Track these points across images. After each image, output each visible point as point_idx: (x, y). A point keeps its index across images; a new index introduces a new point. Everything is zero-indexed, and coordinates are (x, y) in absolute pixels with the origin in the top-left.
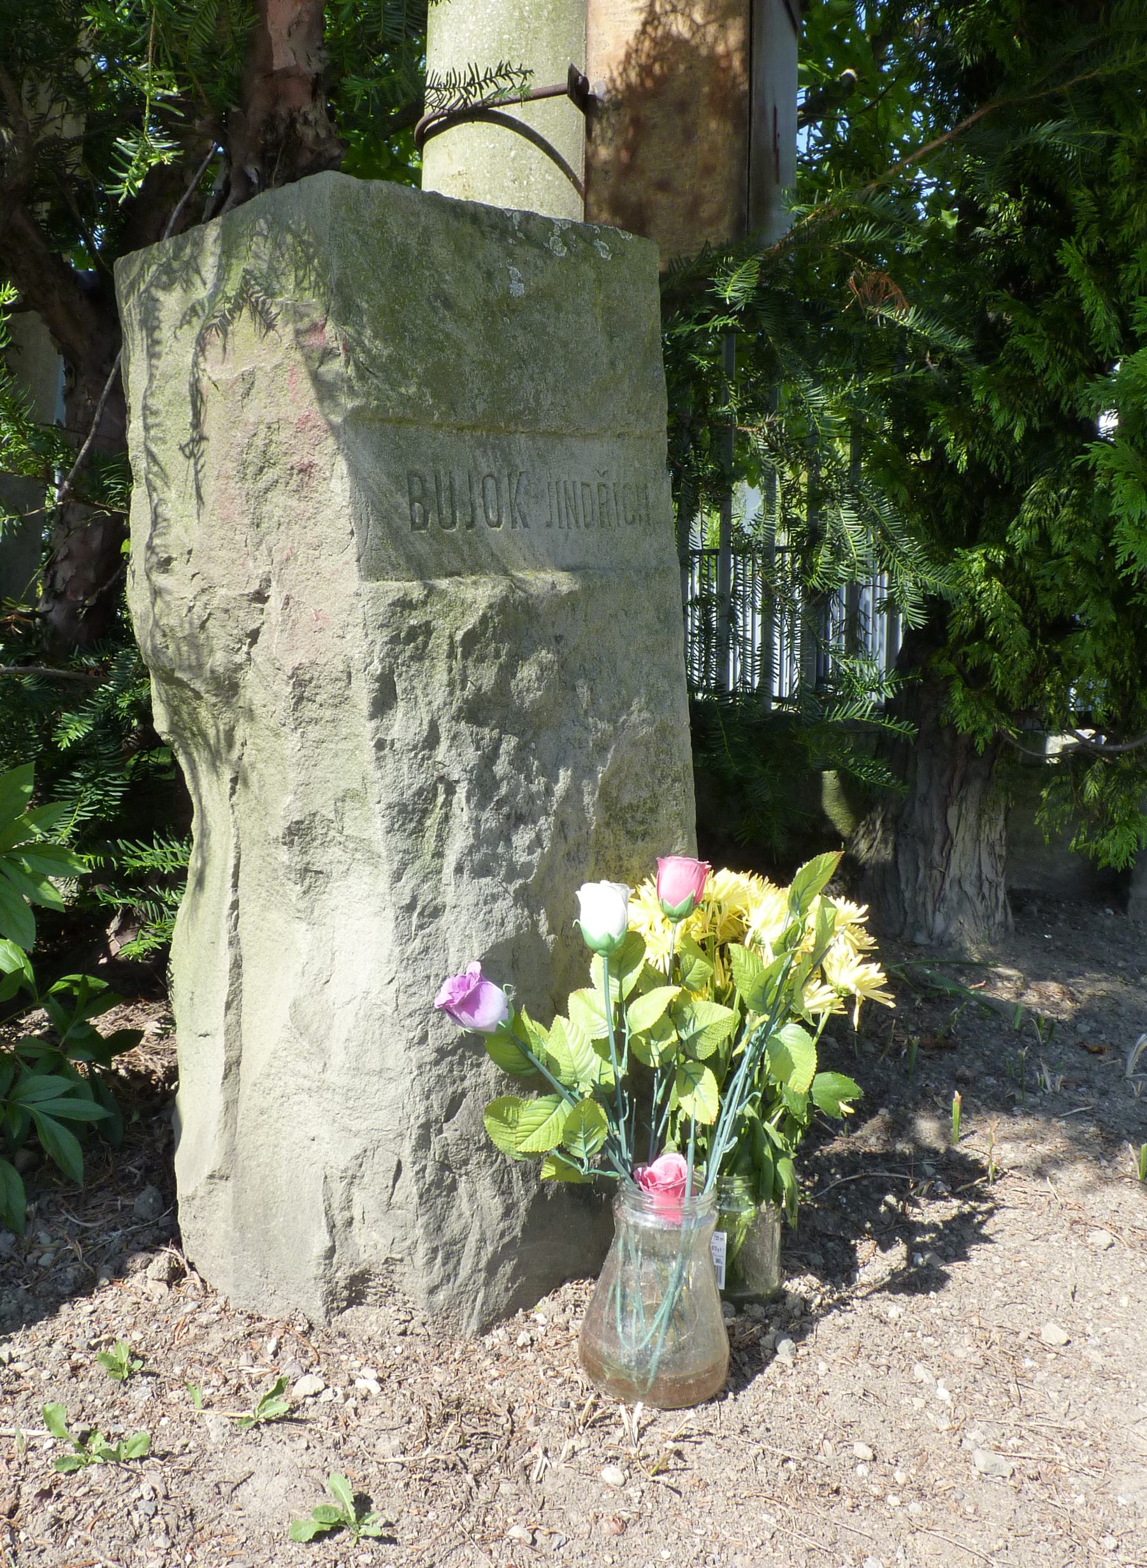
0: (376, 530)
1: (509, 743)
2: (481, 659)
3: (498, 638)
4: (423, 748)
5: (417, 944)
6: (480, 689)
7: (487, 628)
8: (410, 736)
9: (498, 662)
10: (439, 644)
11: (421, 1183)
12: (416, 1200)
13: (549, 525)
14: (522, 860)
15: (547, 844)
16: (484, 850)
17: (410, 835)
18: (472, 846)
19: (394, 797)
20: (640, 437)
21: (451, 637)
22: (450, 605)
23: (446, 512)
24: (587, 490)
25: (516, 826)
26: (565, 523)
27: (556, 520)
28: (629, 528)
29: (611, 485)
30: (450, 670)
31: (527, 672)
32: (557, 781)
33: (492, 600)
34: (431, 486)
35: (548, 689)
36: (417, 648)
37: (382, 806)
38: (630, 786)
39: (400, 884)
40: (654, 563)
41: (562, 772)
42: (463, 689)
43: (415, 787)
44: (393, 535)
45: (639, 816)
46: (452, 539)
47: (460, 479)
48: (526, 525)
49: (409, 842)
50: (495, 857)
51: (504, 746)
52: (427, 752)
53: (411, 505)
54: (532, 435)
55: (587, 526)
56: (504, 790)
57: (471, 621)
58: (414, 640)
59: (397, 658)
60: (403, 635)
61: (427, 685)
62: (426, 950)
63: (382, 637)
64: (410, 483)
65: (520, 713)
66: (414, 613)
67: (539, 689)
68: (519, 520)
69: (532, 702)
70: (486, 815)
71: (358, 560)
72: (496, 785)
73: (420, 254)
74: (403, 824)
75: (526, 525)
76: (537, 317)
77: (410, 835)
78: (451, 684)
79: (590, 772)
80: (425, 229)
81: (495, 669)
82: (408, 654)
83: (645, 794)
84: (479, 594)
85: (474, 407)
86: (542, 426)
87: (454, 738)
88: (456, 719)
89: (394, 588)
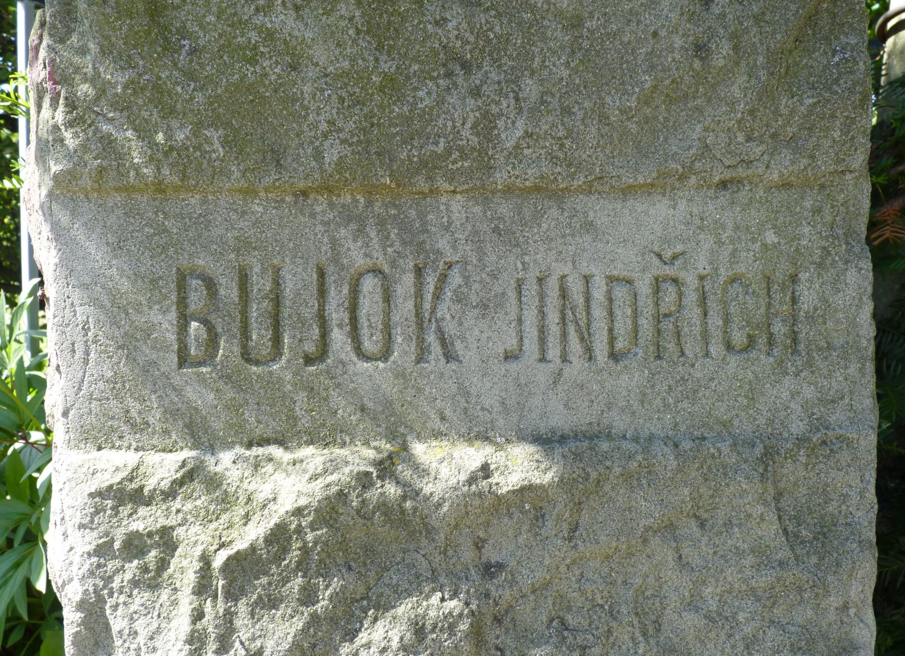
2: (271, 602)
3: (313, 566)
7: (285, 550)
9: (307, 611)
10: (184, 569)
13: (509, 356)
20: (786, 185)
21: (206, 560)
22: (226, 501)
23: (259, 336)
24: (620, 293)
26: (554, 353)
27: (531, 346)
28: (733, 361)
29: (690, 280)
30: (198, 615)
33: (303, 502)
34: (229, 291)
36: (145, 569)
40: (798, 427)
47: (296, 280)
48: (449, 356)
53: (183, 328)
54: (483, 194)
55: (614, 356)
57: (253, 533)
58: (141, 553)
59: (109, 580)
60: (117, 545)
61: (158, 630)
66: (142, 511)
68: (436, 349)
75: (449, 356)
81: (298, 623)
82: (128, 576)
84: (288, 483)
85: (318, 155)
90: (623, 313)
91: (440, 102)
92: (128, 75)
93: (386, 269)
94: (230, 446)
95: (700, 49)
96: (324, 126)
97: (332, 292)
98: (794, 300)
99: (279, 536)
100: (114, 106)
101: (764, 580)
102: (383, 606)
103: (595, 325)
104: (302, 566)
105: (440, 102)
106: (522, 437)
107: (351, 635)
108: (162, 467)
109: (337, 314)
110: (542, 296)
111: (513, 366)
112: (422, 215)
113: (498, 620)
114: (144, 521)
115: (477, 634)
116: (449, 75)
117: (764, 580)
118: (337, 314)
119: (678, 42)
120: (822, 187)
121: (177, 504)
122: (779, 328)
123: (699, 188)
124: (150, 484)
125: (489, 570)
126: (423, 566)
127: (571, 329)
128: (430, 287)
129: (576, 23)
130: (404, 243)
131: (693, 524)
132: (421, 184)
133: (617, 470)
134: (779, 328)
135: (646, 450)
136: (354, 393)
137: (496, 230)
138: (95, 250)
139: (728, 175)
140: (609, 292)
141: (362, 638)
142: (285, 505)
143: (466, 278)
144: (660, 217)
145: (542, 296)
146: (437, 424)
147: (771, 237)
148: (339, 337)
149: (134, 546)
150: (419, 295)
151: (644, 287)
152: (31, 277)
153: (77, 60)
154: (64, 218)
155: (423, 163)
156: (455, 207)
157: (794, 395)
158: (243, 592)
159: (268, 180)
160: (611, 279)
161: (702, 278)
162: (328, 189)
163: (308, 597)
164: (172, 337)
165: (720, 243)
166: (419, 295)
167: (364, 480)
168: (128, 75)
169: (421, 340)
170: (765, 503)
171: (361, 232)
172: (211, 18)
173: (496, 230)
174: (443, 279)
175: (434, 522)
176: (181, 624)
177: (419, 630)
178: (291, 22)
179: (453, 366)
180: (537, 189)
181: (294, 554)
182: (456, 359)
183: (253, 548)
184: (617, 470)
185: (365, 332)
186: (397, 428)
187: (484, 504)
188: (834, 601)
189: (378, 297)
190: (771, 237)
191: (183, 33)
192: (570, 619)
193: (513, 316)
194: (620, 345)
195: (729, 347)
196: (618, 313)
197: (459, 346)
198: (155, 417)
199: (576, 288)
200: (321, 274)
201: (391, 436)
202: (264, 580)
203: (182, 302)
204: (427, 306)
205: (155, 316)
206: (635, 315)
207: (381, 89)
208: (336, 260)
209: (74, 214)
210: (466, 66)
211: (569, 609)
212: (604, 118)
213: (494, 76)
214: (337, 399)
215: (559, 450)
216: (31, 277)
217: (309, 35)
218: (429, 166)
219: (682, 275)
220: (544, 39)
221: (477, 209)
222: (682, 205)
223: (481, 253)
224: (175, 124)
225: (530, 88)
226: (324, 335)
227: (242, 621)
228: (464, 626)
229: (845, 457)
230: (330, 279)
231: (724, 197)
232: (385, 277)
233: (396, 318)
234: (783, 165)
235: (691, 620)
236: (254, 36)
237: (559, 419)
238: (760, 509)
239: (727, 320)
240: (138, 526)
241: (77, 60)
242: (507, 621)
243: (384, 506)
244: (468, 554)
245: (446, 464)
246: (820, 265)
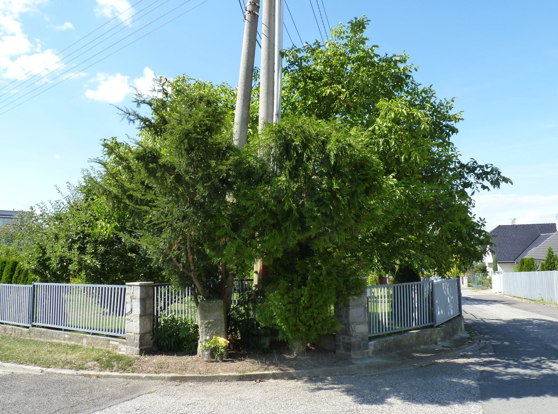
84: (207, 321)
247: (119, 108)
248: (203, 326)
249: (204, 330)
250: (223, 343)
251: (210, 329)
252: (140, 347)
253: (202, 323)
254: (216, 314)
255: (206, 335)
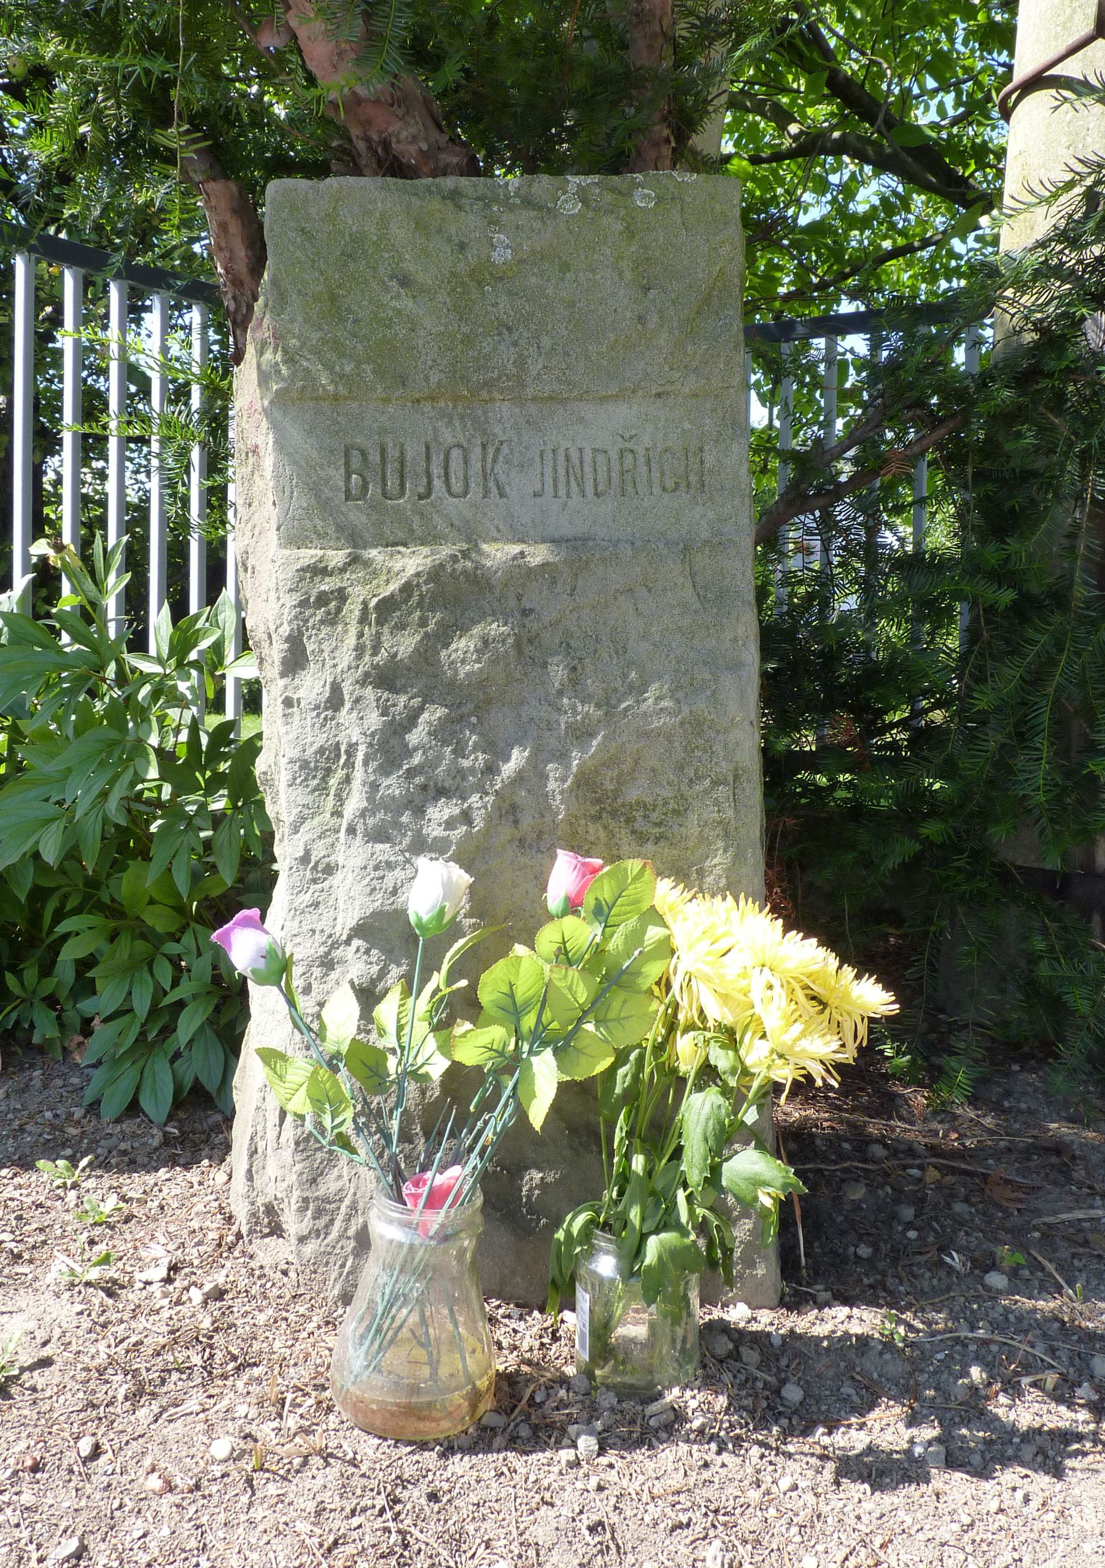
0: (301, 500)
1: (434, 714)
2: (402, 626)
3: (428, 604)
4: (326, 709)
5: (307, 898)
6: (396, 655)
7: (410, 596)
8: (313, 696)
10: (352, 609)
11: (299, 1130)
12: (293, 1146)
14: (435, 833)
15: (479, 823)
16: (380, 815)
17: (314, 790)
18: (365, 809)
19: (295, 753)
21: (365, 603)
22: (375, 574)
23: (392, 483)
24: (600, 458)
25: (436, 799)
26: (562, 492)
27: (549, 489)
28: (666, 496)
29: (641, 451)
30: (361, 635)
31: (463, 645)
32: (507, 759)
33: (420, 569)
34: (375, 457)
35: (494, 662)
36: (329, 613)
37: (286, 760)
38: (643, 781)
39: (297, 836)
40: (705, 535)
41: (515, 752)
42: (375, 653)
43: (316, 746)
44: (324, 506)
45: (655, 816)
46: (398, 510)
47: (414, 451)
49: (310, 798)
50: (397, 825)
51: (425, 716)
52: (329, 713)
55: (597, 495)
56: (417, 759)
57: (394, 587)
58: (326, 604)
59: (307, 621)
61: (336, 648)
62: (316, 905)
63: (291, 600)
64: (347, 455)
65: (452, 683)
66: (327, 579)
67: (478, 661)
68: (494, 491)
69: (468, 674)
70: (391, 780)
71: (278, 529)
72: (409, 753)
73: (380, 239)
74: (306, 780)
76: (533, 280)
77: (314, 790)
78: (359, 649)
79: (563, 757)
80: (382, 215)
82: (318, 618)
83: (666, 793)
84: (411, 562)
85: (427, 379)
86: (530, 392)
87: (357, 701)
88: (363, 682)
89: (309, 555)
90: (602, 470)
91: (495, 349)
92: (319, 335)
93: (465, 445)
94: (376, 546)
95: (641, 319)
96: (430, 363)
97: (434, 458)
98: (702, 462)
99: (407, 588)
100: (310, 351)
101: (686, 621)
102: (465, 630)
103: (586, 476)
104: (420, 604)
105: (495, 349)
106: (544, 541)
107: (447, 646)
108: (337, 557)
109: (436, 470)
110: (555, 460)
111: (538, 500)
112: (485, 413)
113: (530, 641)
114: (327, 585)
115: (518, 646)
116: (500, 334)
117: (686, 621)
118: (436, 470)
119: (628, 315)
120: (716, 396)
121: (348, 575)
122: (693, 478)
123: (644, 397)
124: (331, 565)
125: (525, 613)
126: (487, 608)
127: (572, 478)
128: (491, 451)
129: (571, 305)
130: (475, 429)
131: (645, 590)
132: (484, 394)
133: (598, 556)
134: (693, 478)
135: (615, 546)
136: (447, 516)
137: (528, 422)
138: (296, 435)
139: (660, 390)
140: (594, 457)
141: (453, 646)
142: (411, 571)
143: (511, 450)
144: (622, 413)
145: (555, 460)
146: (495, 534)
147: (687, 425)
148: (438, 483)
149: (323, 599)
150: (484, 460)
151: (614, 455)
152: (24, 574)
153: (289, 326)
154: (278, 415)
155: (486, 383)
156: (504, 409)
157: (703, 516)
158: (386, 621)
159: (398, 393)
160: (595, 450)
161: (647, 449)
162: (432, 398)
163: (423, 622)
164: (341, 484)
165: (657, 429)
166: (484, 460)
167: (454, 558)
168: (319, 335)
169: (485, 487)
170: (685, 577)
171: (450, 422)
172: (365, 303)
173: (528, 422)
174: (498, 450)
175: (493, 582)
176: (351, 641)
177: (486, 642)
178: (410, 304)
179: (505, 500)
180: (551, 398)
181: (415, 599)
182: (506, 496)
183: (392, 595)
184: (598, 556)
185: (453, 480)
186: (472, 538)
187: (521, 574)
188: (728, 635)
189: (461, 461)
190: (687, 425)
191: (349, 311)
192: (572, 643)
193: (539, 471)
194: (600, 488)
195: (664, 489)
196: (599, 470)
197: (507, 488)
198: (331, 530)
199: (574, 455)
200: (428, 448)
201: (469, 540)
202: (398, 613)
203: (347, 464)
204: (489, 466)
205: (331, 472)
206: (609, 470)
207: (462, 342)
208: (436, 439)
209: (285, 413)
210: (509, 329)
211: (572, 637)
212: (588, 358)
213: (525, 334)
214: (437, 520)
215: (564, 545)
216: (24, 574)
217: (421, 312)
218: (489, 384)
219: (635, 447)
220: (554, 313)
221: (517, 410)
222: (635, 407)
223: (519, 434)
224: (344, 361)
225: (546, 342)
226: (430, 482)
227: (386, 637)
228: (511, 641)
229: (732, 551)
230: (433, 450)
231: (659, 402)
232: (464, 450)
233: (471, 472)
234: (692, 384)
235: (644, 646)
236: (390, 313)
237: (566, 530)
238: (681, 580)
239: (663, 474)
240: (324, 587)
241: (289, 326)
242: (536, 642)
243: (464, 572)
244: (513, 602)
245: (498, 553)
246: (716, 441)
247: (138, 1088)
248: (339, 653)
249: (358, 725)
250: (775, 1012)
251: (471, 708)
252: (558, 167)
253: (320, 603)
254: (608, 425)
255: (393, 826)
